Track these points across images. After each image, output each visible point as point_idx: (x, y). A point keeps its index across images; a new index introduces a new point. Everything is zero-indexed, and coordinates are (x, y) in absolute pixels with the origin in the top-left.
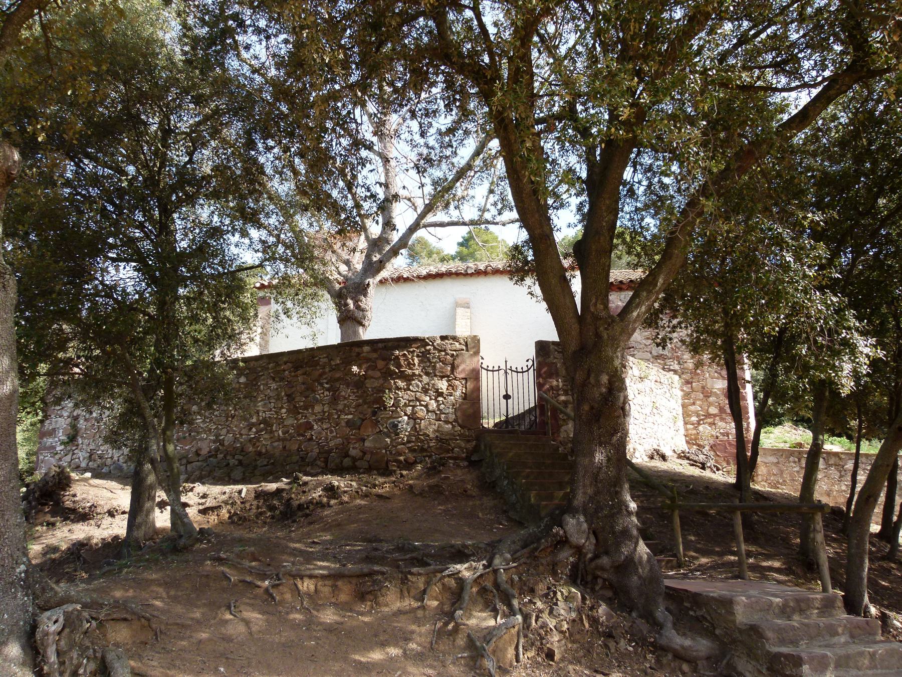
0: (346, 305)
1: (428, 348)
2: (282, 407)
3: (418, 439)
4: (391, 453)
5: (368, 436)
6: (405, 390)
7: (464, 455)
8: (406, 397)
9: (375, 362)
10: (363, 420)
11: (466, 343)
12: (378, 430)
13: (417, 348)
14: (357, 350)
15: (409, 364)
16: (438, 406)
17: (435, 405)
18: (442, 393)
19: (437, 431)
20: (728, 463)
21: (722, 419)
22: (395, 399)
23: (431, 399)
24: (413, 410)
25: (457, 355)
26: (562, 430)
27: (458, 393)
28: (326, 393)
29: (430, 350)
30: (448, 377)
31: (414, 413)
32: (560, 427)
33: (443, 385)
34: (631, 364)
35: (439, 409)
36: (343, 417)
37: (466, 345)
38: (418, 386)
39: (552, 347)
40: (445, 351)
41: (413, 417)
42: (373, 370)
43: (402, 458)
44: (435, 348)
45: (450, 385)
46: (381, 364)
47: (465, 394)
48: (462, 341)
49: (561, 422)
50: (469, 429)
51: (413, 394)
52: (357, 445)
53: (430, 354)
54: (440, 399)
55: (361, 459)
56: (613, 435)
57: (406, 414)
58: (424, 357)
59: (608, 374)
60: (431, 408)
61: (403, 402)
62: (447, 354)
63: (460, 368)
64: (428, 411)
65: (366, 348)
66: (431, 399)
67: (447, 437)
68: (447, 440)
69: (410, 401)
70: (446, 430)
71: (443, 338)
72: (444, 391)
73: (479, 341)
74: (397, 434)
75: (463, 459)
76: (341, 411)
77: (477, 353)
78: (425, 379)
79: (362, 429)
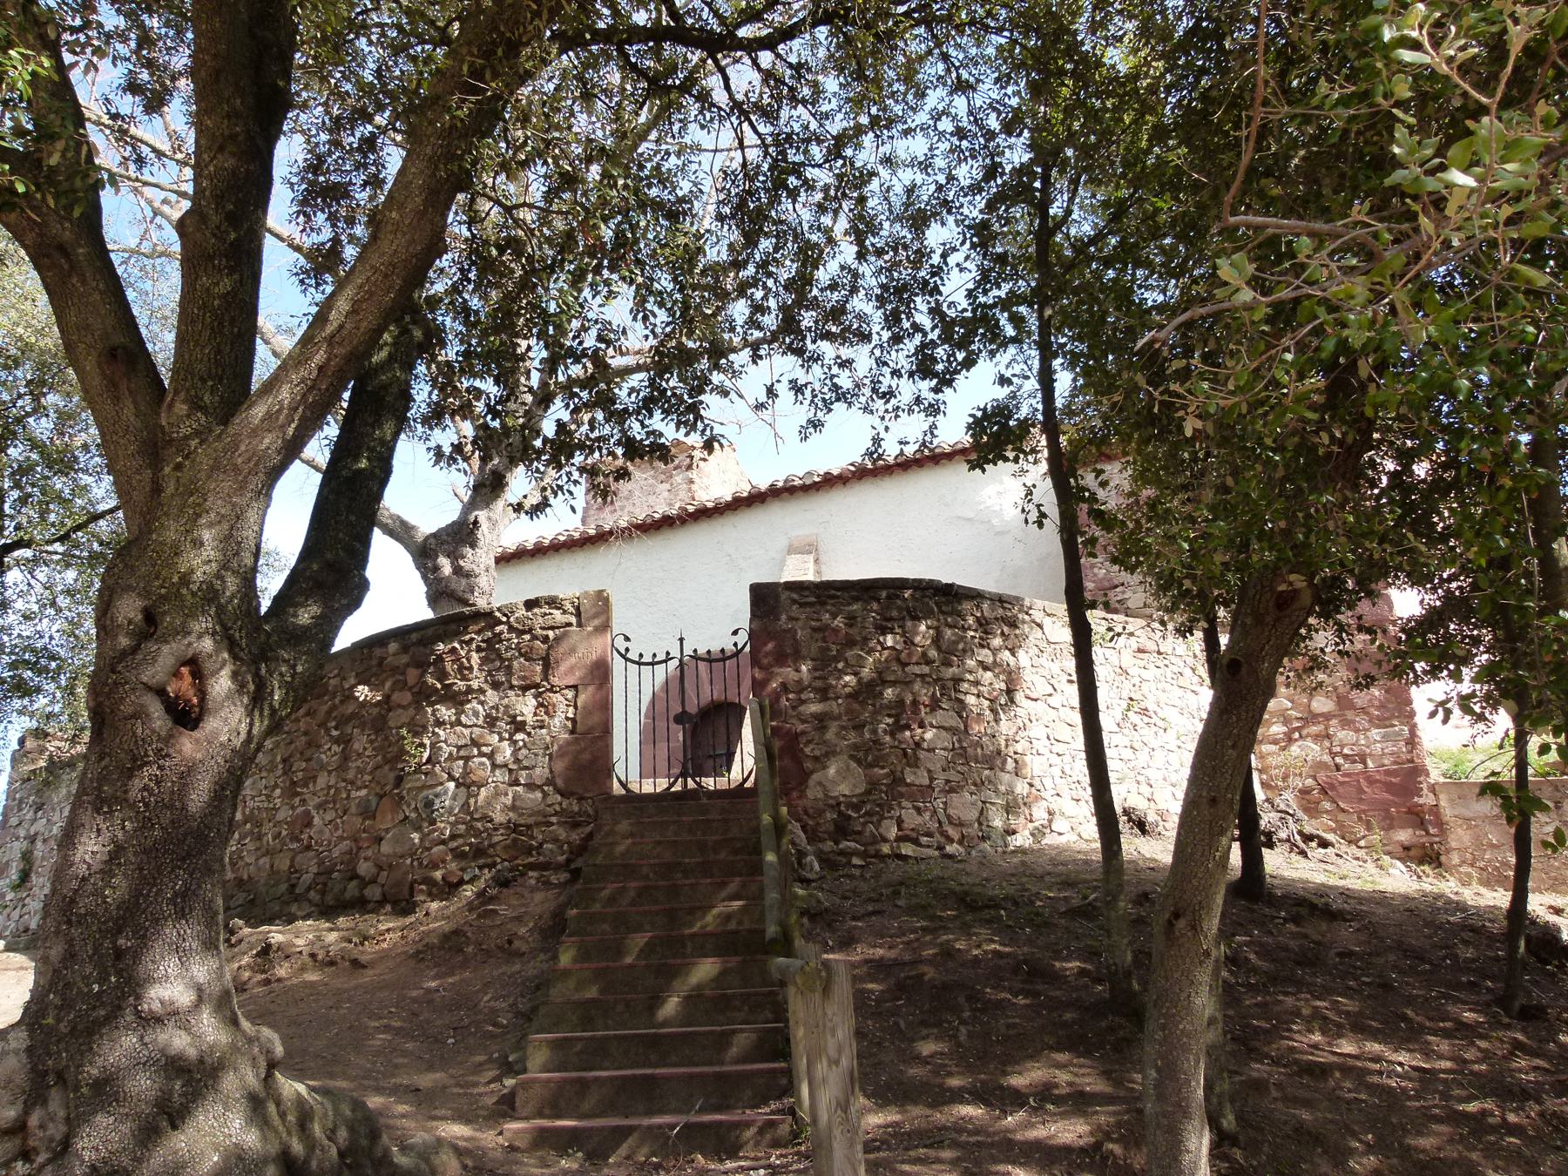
0: (436, 569)
1: (498, 629)
2: (276, 786)
3: (470, 828)
4: (421, 864)
5: (387, 831)
6: (452, 725)
7: (561, 859)
8: (453, 739)
9: (403, 673)
10: (381, 797)
11: (578, 609)
12: (401, 817)
13: (478, 632)
14: (378, 652)
15: (461, 668)
16: (515, 753)
17: (508, 752)
18: (524, 723)
19: (513, 808)
20: (1369, 827)
21: (1346, 724)
22: (433, 745)
23: (501, 739)
24: (465, 765)
25: (557, 639)
26: (811, 782)
27: (557, 721)
28: (335, 748)
29: (501, 633)
30: (537, 686)
31: (467, 772)
32: (805, 776)
33: (526, 706)
34: (1038, 615)
35: (517, 761)
36: (354, 794)
37: (578, 614)
38: (476, 714)
39: (784, 596)
40: (530, 631)
41: (467, 784)
42: (402, 689)
43: (438, 875)
44: (511, 629)
45: (541, 705)
46: (412, 675)
47: (574, 721)
48: (568, 607)
49: (808, 765)
50: (581, 799)
51: (466, 732)
52: (369, 853)
53: (501, 641)
54: (519, 736)
55: (374, 881)
56: (130, 774)
57: (451, 778)
58: (491, 650)
59: (145, 593)
60: (499, 759)
61: (446, 750)
62: (535, 638)
63: (563, 668)
64: (494, 766)
65: (393, 647)
66: (501, 739)
67: (531, 821)
68: (529, 827)
69: (459, 748)
70: (530, 805)
71: (530, 604)
72: (529, 719)
73: (606, 601)
74: (433, 822)
75: (558, 868)
76: (352, 783)
77: (605, 627)
78: (492, 696)
79: (378, 818)
